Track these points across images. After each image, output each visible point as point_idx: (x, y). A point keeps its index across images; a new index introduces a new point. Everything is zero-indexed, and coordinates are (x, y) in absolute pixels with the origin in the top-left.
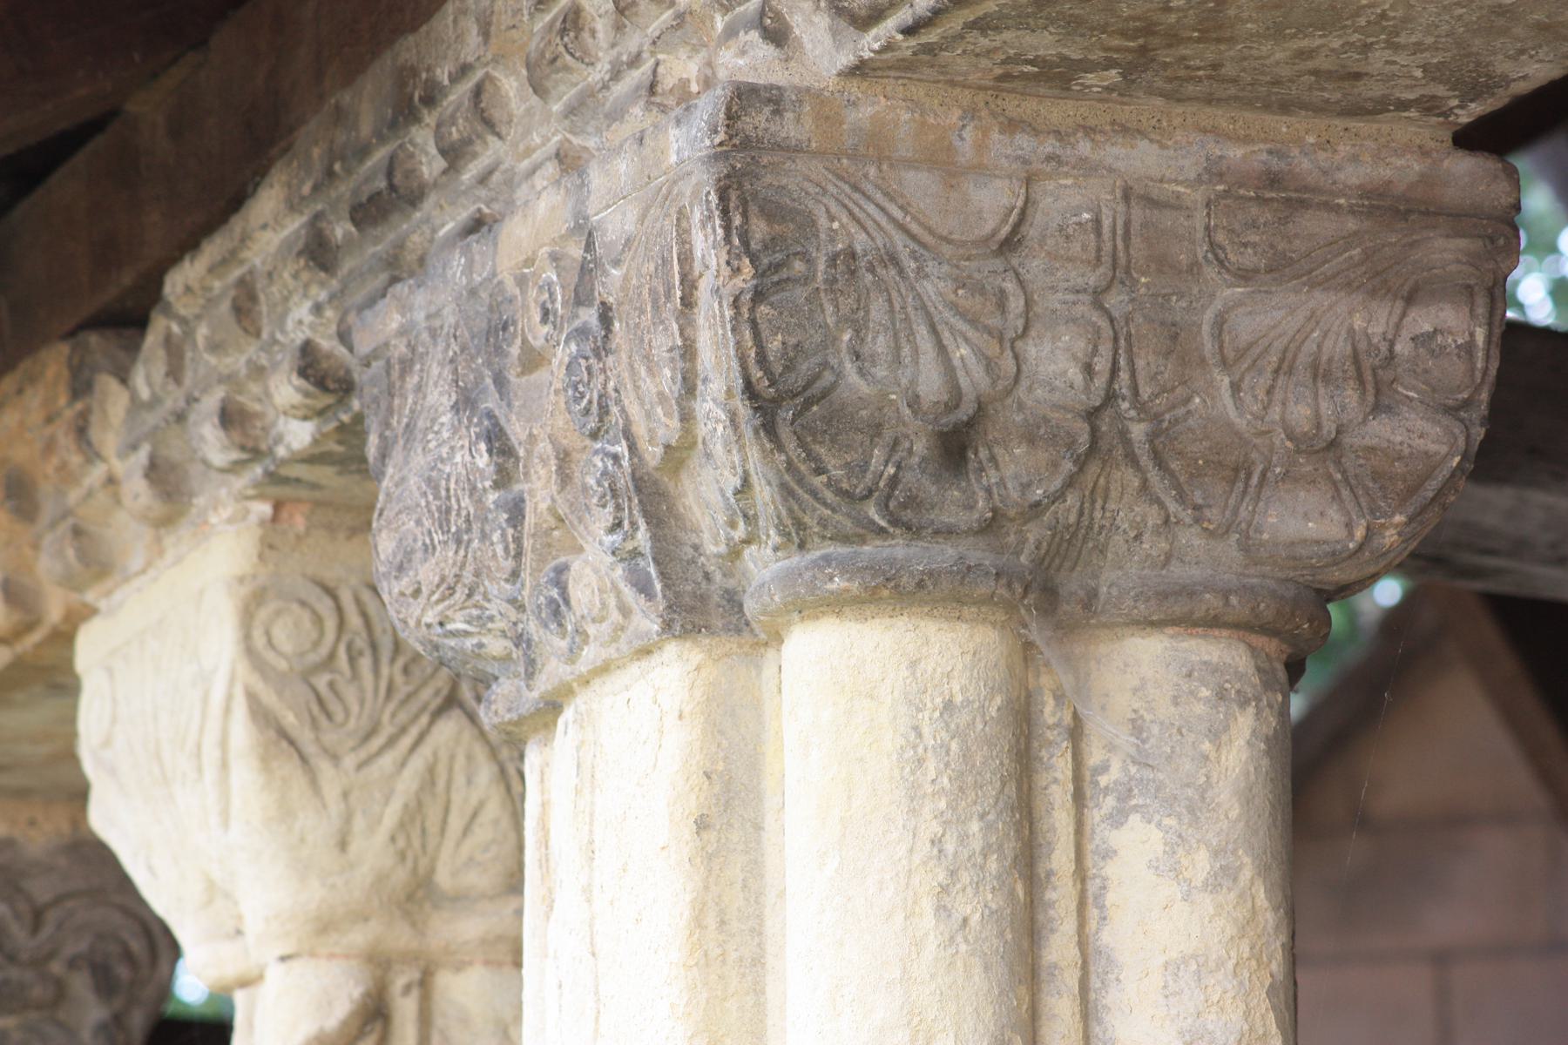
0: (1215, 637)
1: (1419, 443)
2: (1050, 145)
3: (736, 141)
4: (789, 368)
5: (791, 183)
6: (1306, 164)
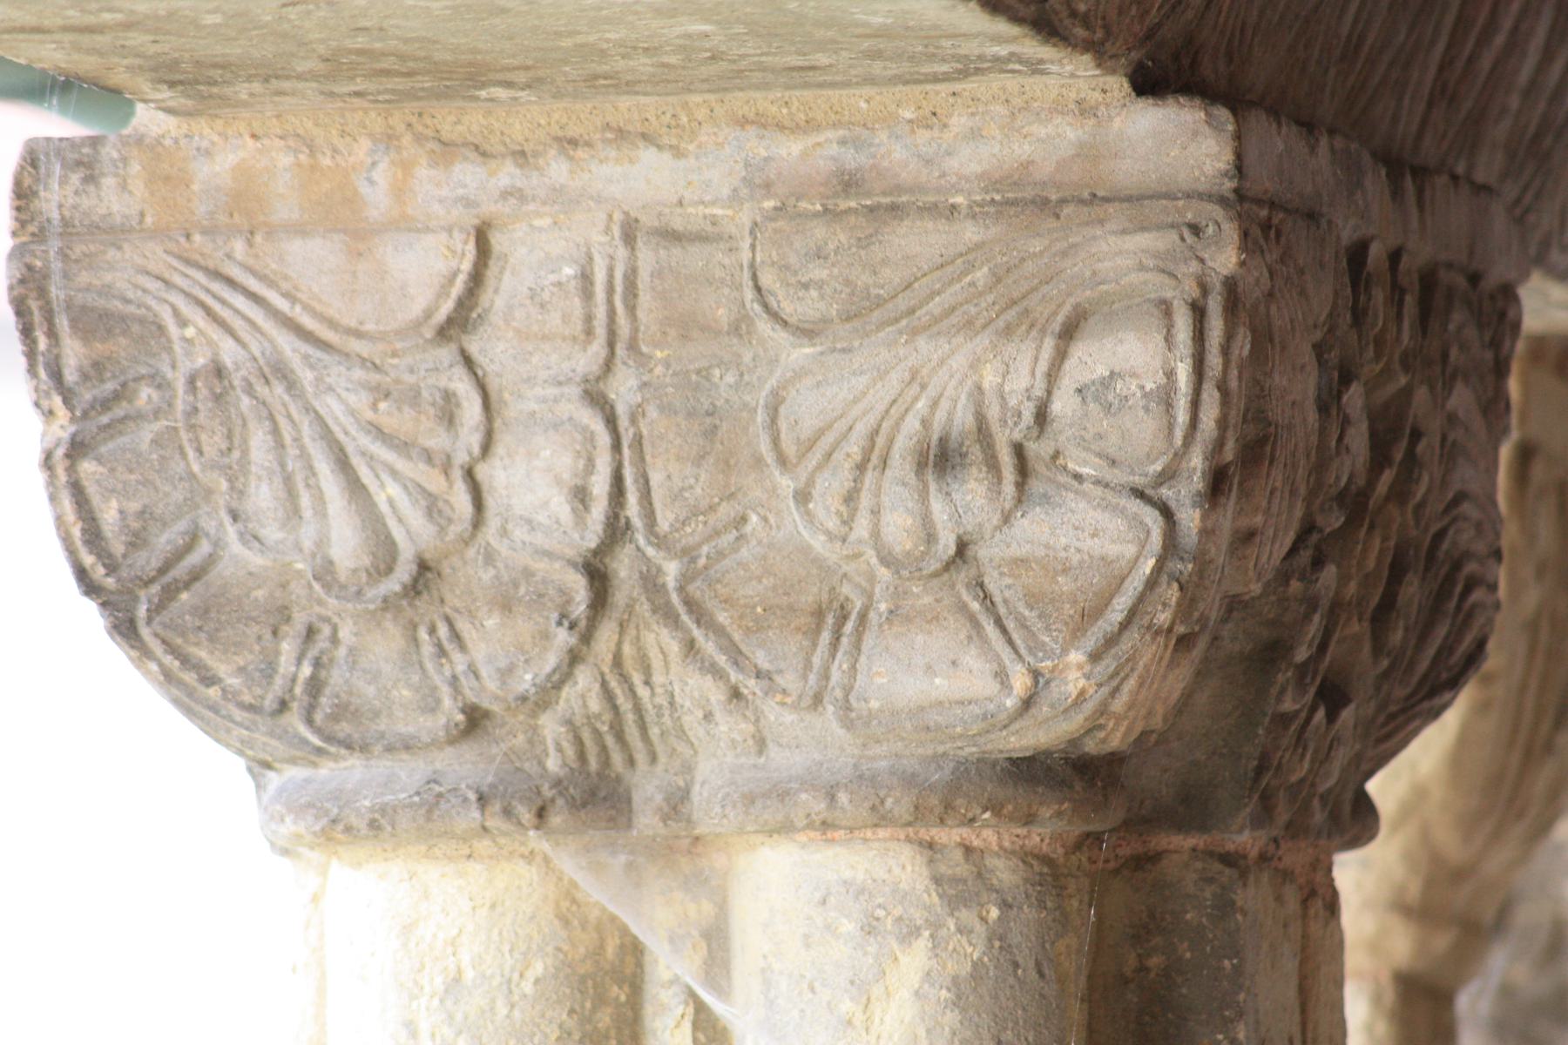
0: (865, 840)
1: (1090, 544)
2: (508, 174)
3: (32, 228)
4: (137, 541)
5: (120, 280)
6: (899, 153)
